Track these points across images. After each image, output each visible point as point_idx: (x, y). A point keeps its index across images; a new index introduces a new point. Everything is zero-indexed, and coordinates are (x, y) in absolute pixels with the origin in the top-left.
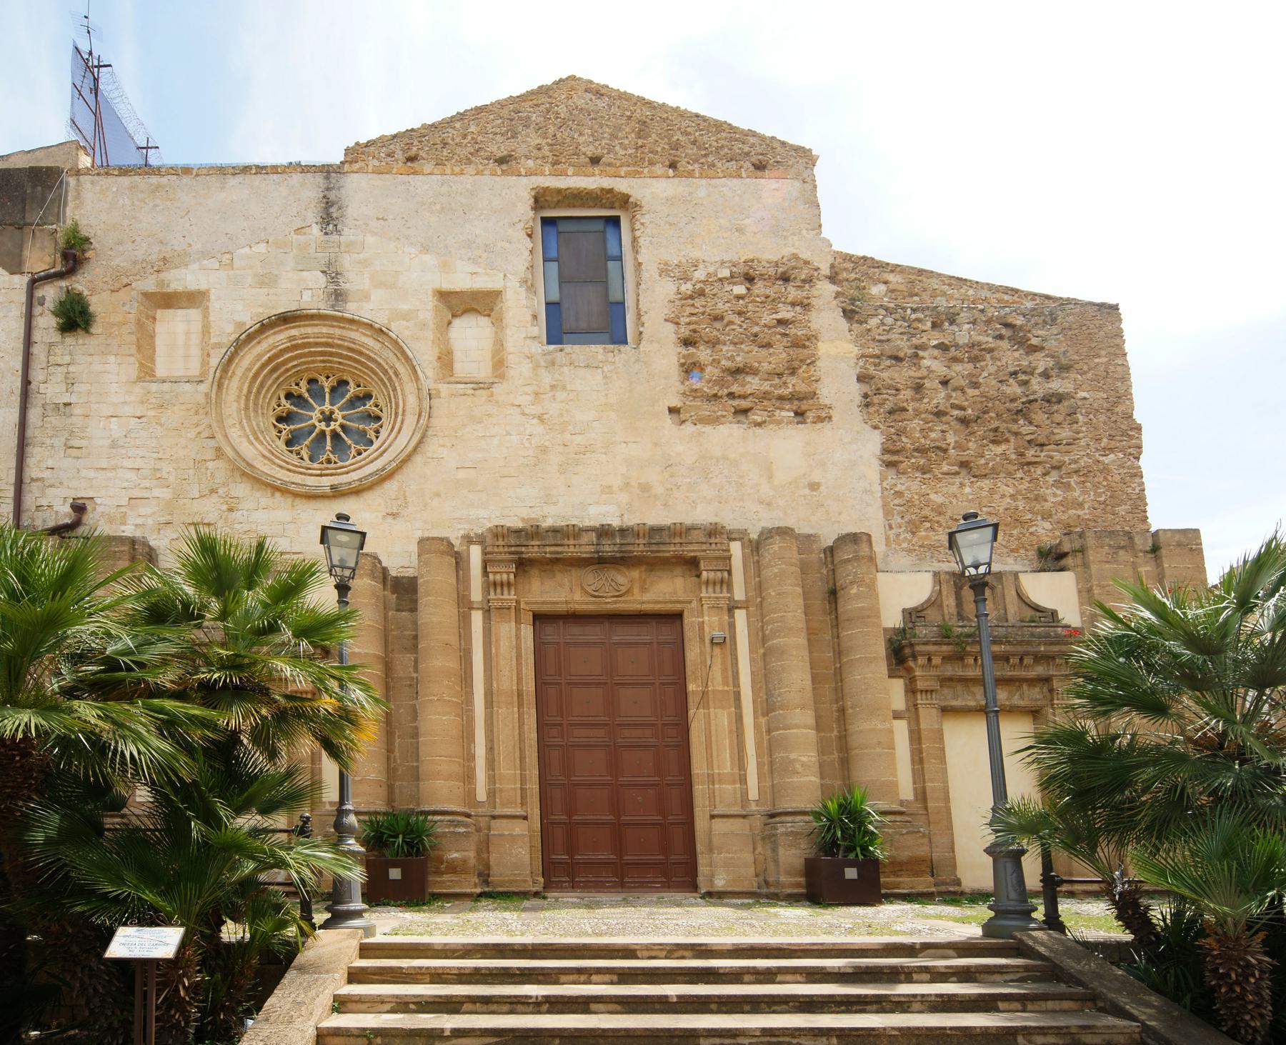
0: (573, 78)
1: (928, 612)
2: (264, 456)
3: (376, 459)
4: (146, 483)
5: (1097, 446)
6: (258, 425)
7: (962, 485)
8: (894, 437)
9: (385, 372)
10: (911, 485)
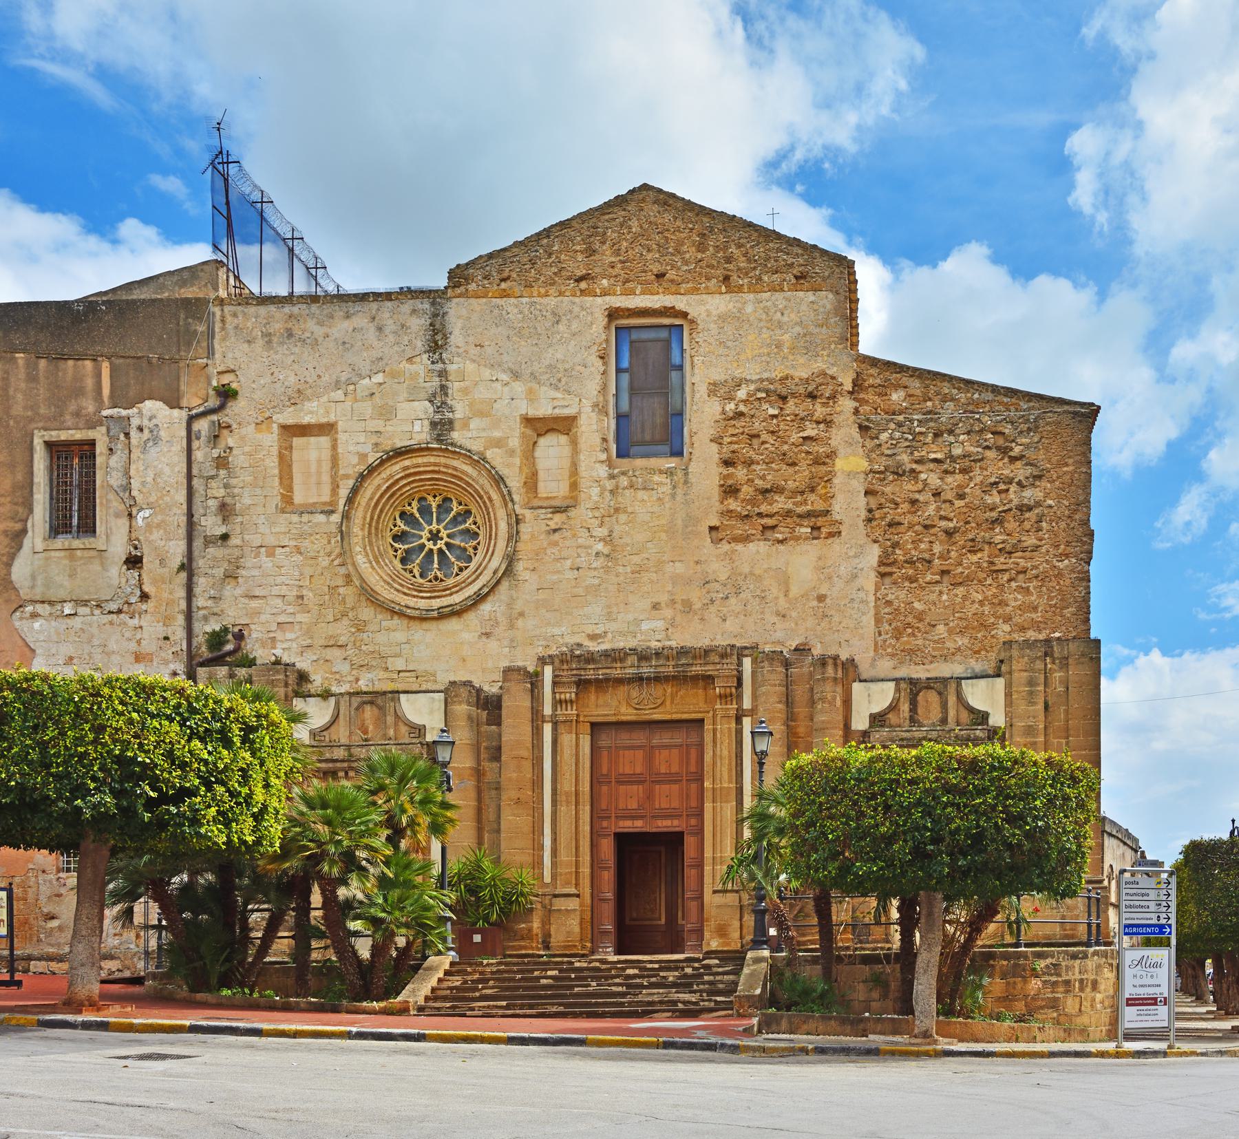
0: (645, 187)
1: (890, 716)
2: (385, 581)
3: (474, 581)
4: (291, 609)
5: (1055, 552)
6: (379, 550)
7: (941, 593)
8: (890, 549)
9: (481, 498)
10: (898, 595)
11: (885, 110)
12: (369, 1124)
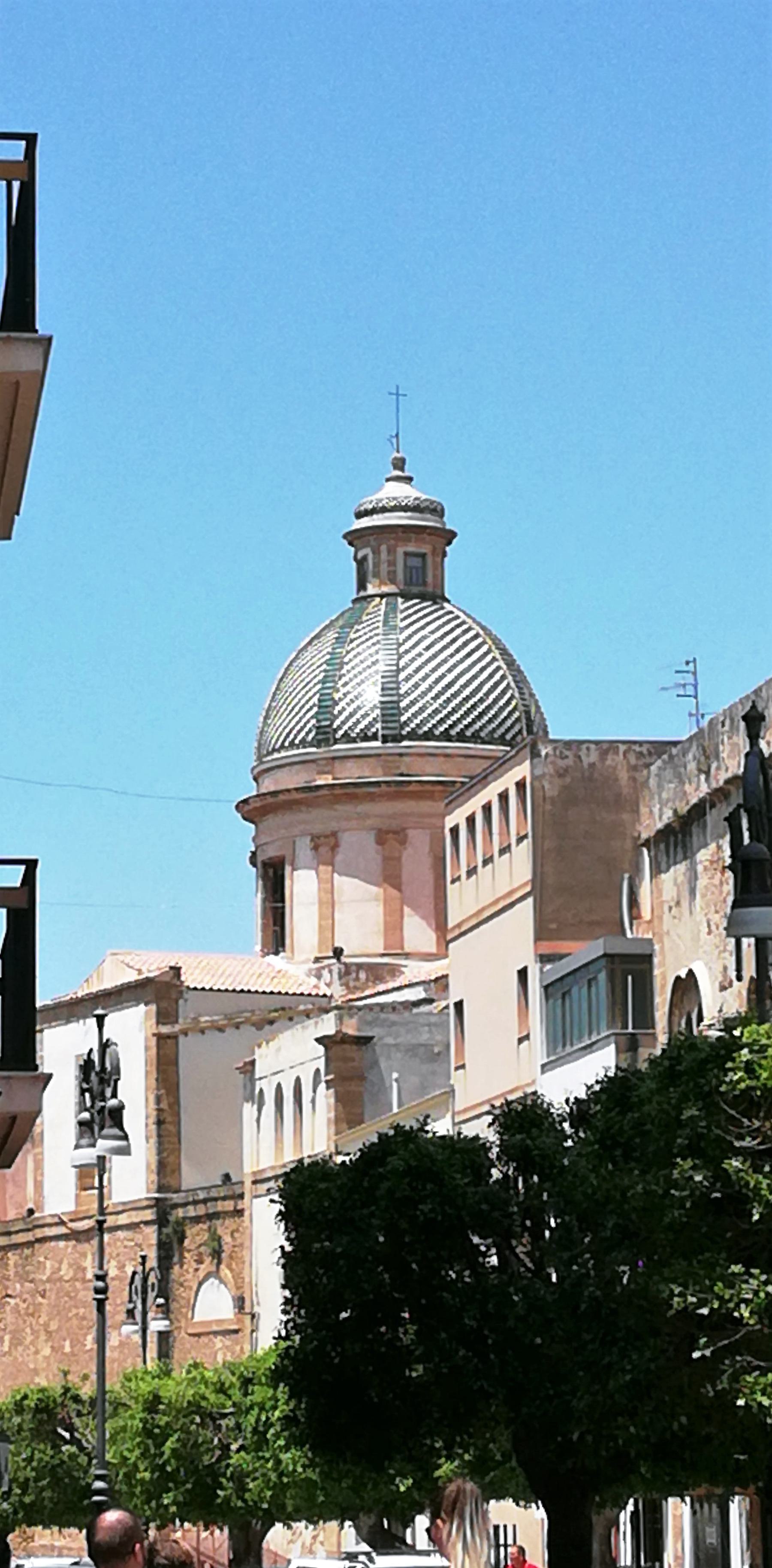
11: (293, 1451)
12: (57, 1544)
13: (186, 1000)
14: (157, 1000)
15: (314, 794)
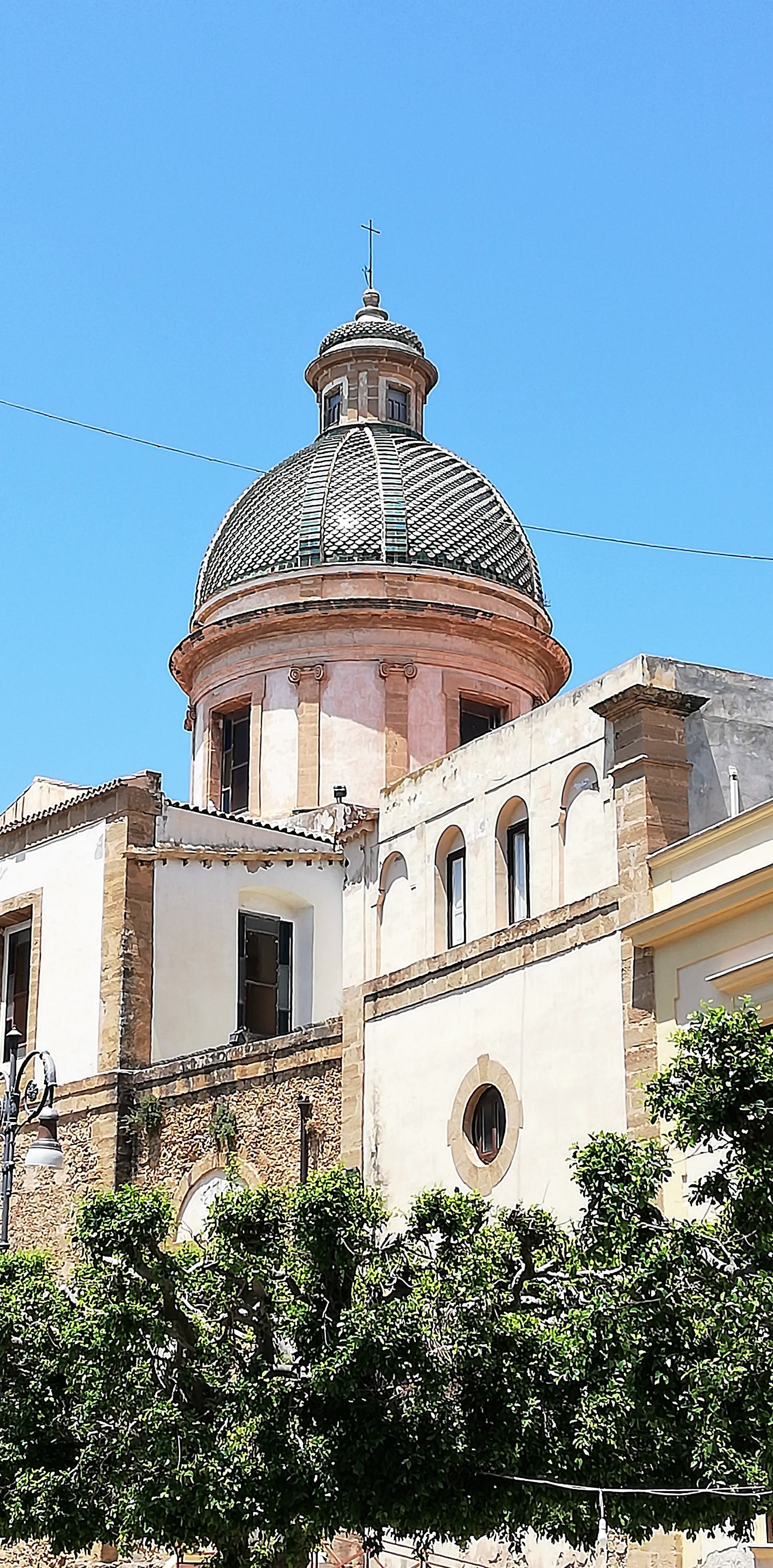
13: (165, 818)
14: (131, 810)
15: (301, 615)
